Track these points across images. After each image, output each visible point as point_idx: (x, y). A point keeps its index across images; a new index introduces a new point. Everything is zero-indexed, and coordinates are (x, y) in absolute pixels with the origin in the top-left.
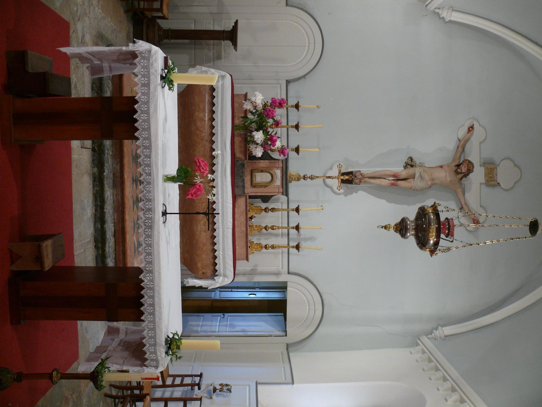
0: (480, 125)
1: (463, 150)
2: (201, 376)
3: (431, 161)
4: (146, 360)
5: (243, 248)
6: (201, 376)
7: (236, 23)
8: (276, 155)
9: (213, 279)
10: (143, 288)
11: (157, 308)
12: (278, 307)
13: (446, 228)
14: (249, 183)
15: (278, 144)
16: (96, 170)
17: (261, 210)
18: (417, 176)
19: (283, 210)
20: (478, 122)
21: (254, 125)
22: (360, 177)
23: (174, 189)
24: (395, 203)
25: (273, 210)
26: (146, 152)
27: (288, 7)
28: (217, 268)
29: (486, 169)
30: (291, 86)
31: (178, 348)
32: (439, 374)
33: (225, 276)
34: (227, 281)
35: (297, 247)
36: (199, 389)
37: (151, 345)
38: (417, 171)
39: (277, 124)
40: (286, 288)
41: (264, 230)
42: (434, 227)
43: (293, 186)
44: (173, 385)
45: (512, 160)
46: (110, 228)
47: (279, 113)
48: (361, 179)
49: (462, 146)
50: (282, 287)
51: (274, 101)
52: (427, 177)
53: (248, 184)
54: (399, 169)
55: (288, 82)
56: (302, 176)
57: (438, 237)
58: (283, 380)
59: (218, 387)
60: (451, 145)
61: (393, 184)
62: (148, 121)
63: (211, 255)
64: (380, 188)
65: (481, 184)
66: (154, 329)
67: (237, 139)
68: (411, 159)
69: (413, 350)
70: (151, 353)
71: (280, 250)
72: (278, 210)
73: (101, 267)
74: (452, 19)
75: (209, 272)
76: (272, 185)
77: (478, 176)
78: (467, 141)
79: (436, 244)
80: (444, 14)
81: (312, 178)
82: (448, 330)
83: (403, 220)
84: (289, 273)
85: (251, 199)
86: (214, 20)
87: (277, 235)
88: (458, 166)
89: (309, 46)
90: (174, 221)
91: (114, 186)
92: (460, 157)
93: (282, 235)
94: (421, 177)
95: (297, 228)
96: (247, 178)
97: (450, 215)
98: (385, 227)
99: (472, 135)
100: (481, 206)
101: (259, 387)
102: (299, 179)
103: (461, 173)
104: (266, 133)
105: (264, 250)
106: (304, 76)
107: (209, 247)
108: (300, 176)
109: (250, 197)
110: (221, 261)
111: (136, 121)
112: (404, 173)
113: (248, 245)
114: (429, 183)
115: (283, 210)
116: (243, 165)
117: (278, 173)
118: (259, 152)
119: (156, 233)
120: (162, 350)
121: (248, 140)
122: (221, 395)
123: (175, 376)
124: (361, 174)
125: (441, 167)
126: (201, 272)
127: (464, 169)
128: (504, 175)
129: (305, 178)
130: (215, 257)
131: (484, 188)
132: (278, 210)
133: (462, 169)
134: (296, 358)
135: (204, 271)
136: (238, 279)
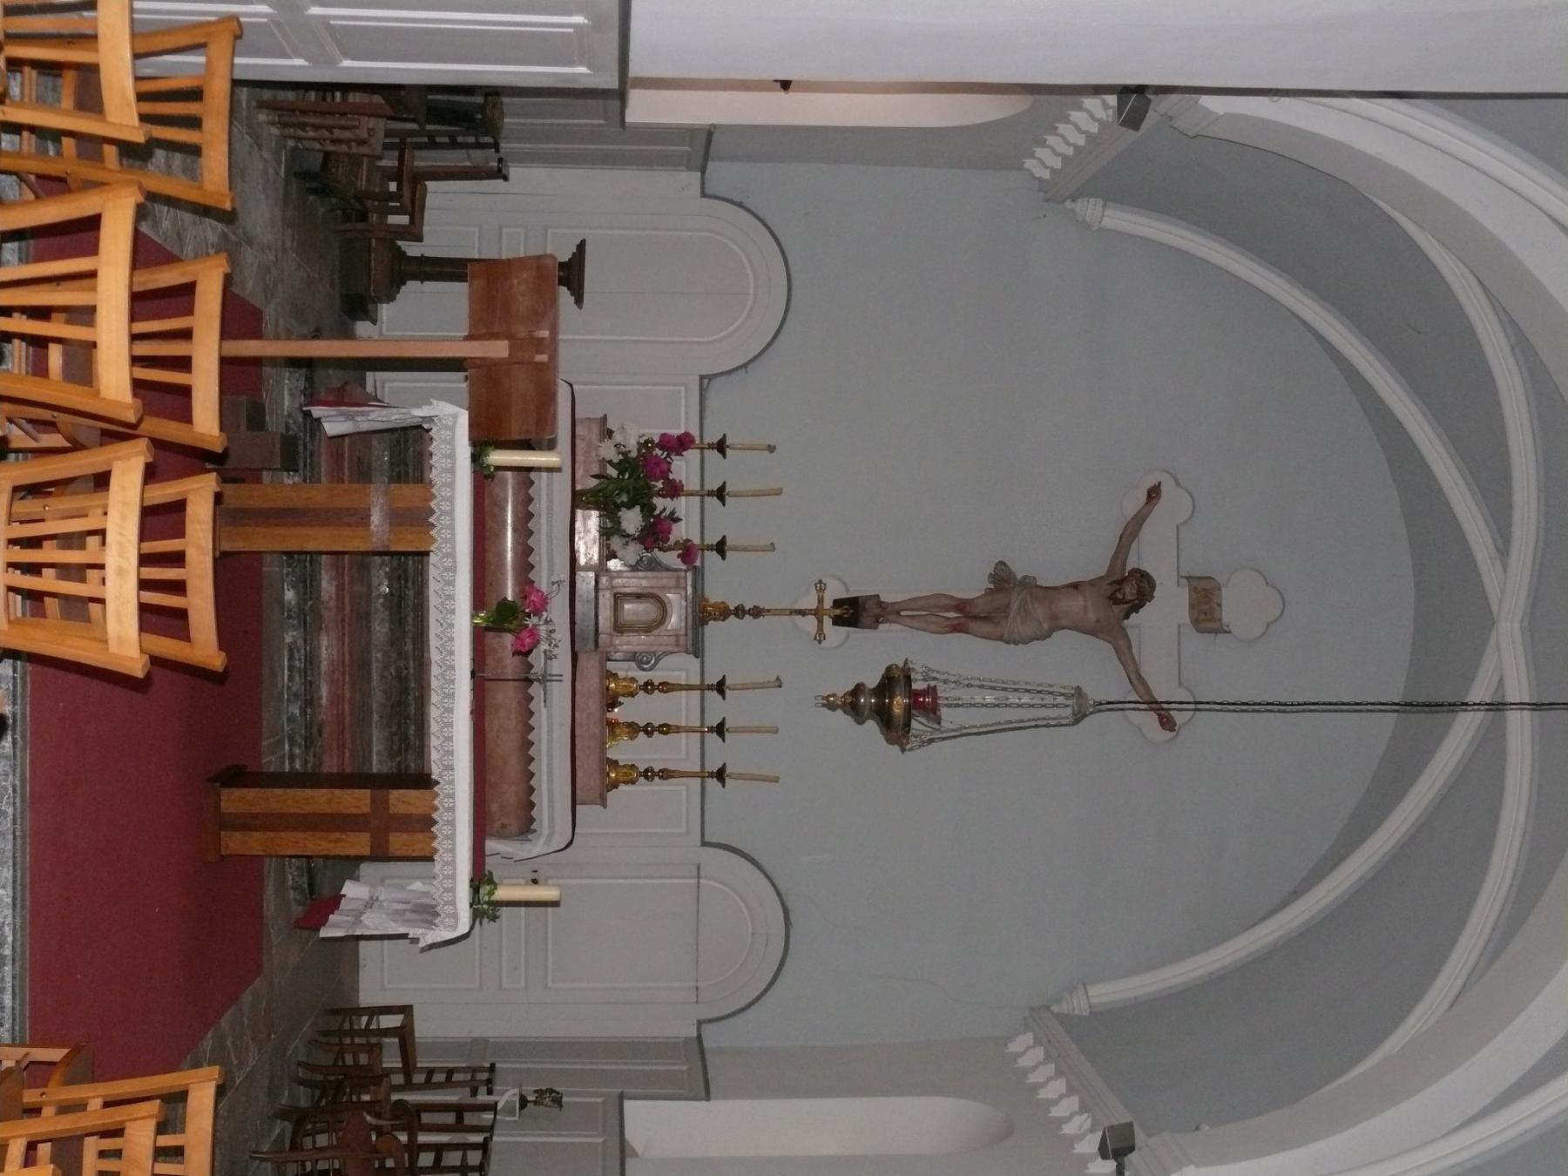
0: (1178, 484)
7: (581, 246)
13: (926, 704)
14: (74, 16)
22: (877, 611)
29: (1193, 590)
39: (674, 490)
47: (684, 468)
55: (705, 380)
81: (757, 612)
100: (1180, 684)
104: (648, 509)
108: (727, 608)
123: (430, 1072)
126: (498, 824)
127: (1129, 591)
130: (531, 790)
135: (505, 821)
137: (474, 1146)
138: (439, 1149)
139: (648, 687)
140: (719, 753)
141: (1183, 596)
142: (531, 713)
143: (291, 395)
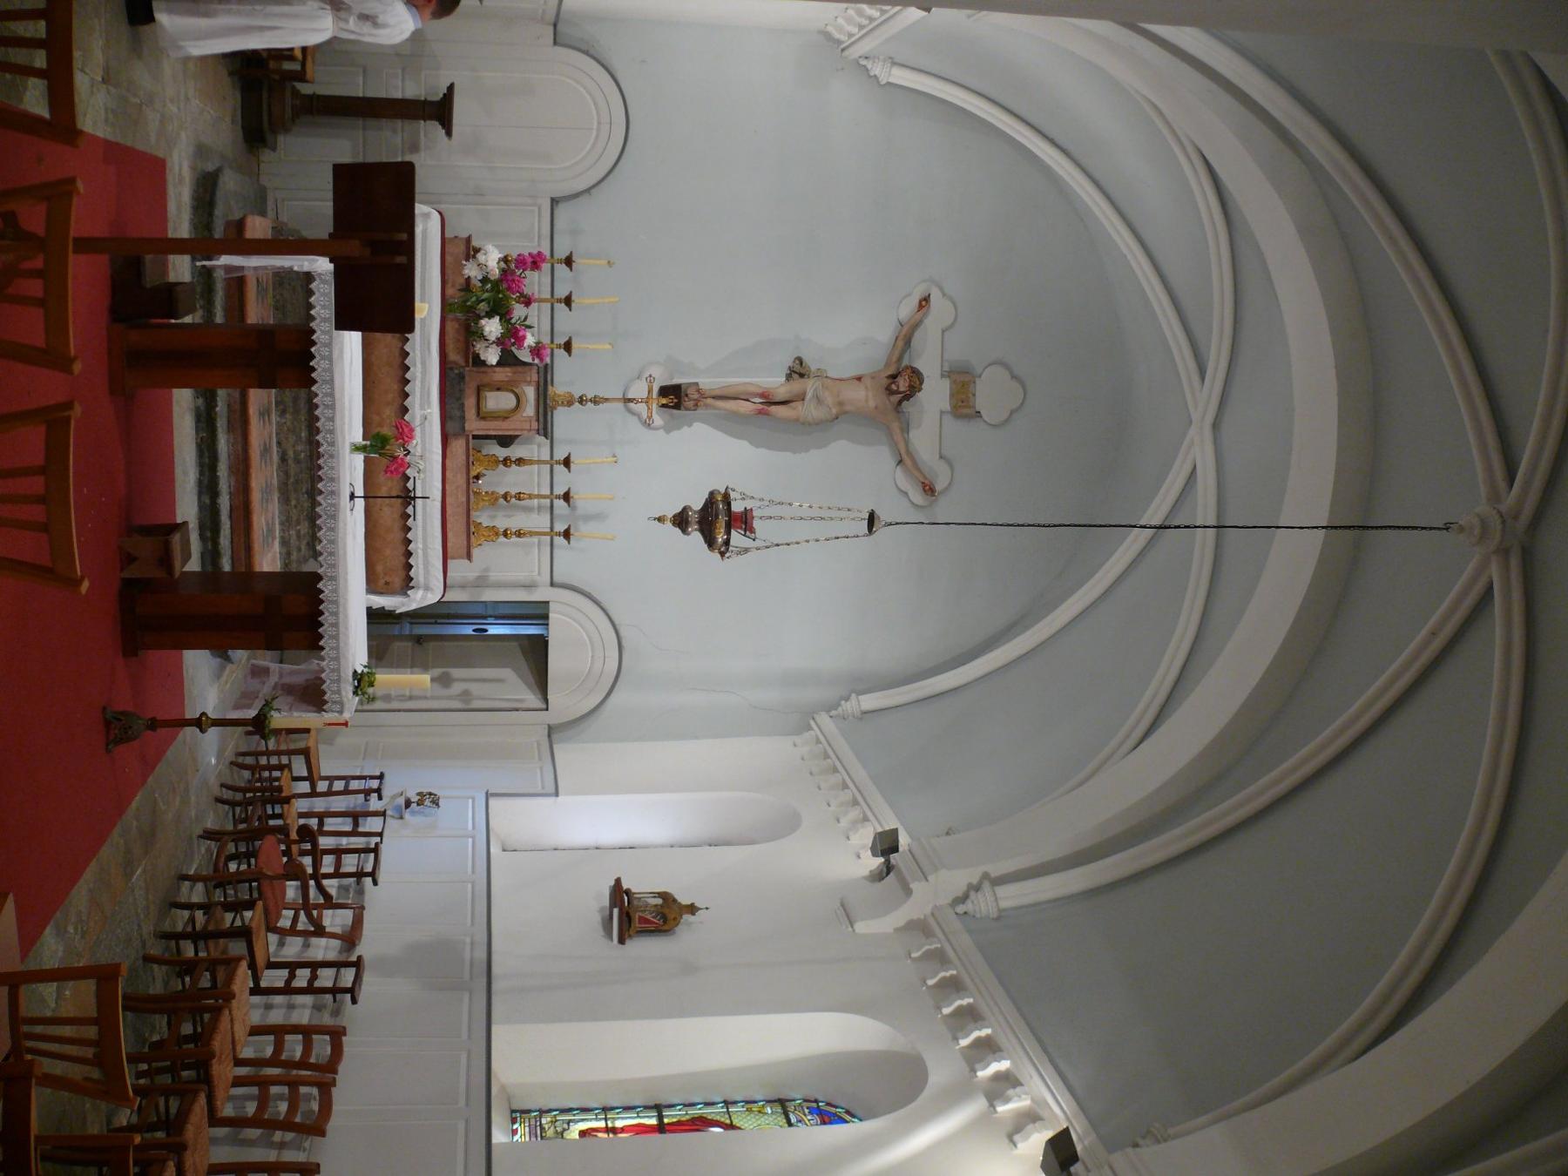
1: (908, 342)
2: (381, 777)
3: (841, 366)
4: (326, 702)
5: (463, 535)
6: (381, 777)
7: (451, 88)
8: (525, 356)
9: (406, 594)
10: (322, 602)
11: (342, 629)
12: (536, 653)
14: (474, 411)
15: (530, 340)
16: (200, 401)
17: (497, 462)
18: (809, 395)
19: (539, 462)
20: (941, 289)
21: (483, 306)
22: (696, 396)
23: (359, 459)
24: (769, 448)
25: (520, 462)
26: (328, 413)
27: (559, 49)
28: (412, 573)
29: (954, 382)
30: (561, 210)
31: (371, 684)
32: (835, 779)
33: (427, 588)
34: (432, 598)
35: (567, 534)
36: (380, 798)
37: (333, 681)
38: (810, 386)
40: (546, 617)
41: (502, 500)
42: (722, 519)
43: (562, 419)
44: (330, 793)
45: (1006, 366)
46: (224, 502)
47: (535, 282)
48: (697, 401)
49: (906, 338)
50: (539, 613)
51: (521, 262)
52: (830, 400)
53: (471, 413)
54: (774, 381)
55: (554, 202)
56: (577, 397)
57: (728, 533)
58: (539, 790)
59: (415, 799)
60: (885, 335)
61: (760, 412)
62: (330, 370)
63: (401, 549)
64: (734, 416)
65: (942, 413)
66: (337, 659)
67: (450, 327)
68: (800, 360)
69: (798, 739)
70: (334, 692)
71: (535, 539)
72: (531, 462)
73: (210, 574)
74: (892, 80)
75: (397, 581)
76: (517, 416)
77: (935, 395)
78: (916, 326)
79: (727, 543)
80: (877, 69)
81: (596, 401)
82: (869, 701)
83: (685, 509)
84: (552, 584)
85: (474, 439)
86: (403, 69)
87: (529, 509)
88: (894, 377)
89: (598, 130)
90: (360, 504)
91: (230, 428)
92: (900, 359)
93: (540, 508)
94: (819, 400)
95: (567, 497)
96: (470, 402)
97: (749, 504)
98: (660, 519)
99: (925, 315)
101: (492, 802)
102: (570, 403)
103: (898, 392)
105: (502, 539)
106: (588, 191)
107: (398, 535)
109: (475, 437)
110: (420, 561)
111: (313, 369)
112: (782, 392)
113: (471, 530)
114: (834, 411)
115: (539, 462)
116: (462, 377)
117: (530, 392)
118: (492, 356)
119: (341, 525)
120: (348, 689)
121: (471, 333)
122: (419, 813)
123: (331, 779)
124: (698, 391)
125: (859, 379)
127: (903, 384)
128: (990, 394)
129: (581, 401)
131: (948, 419)
132: (531, 462)
133: (900, 384)
134: (566, 753)
135: (388, 579)
136: (452, 596)
137: (367, 851)
138: (338, 852)
139: (506, 462)
140: (563, 481)
141: (945, 386)
142: (411, 567)
143: (144, 871)
